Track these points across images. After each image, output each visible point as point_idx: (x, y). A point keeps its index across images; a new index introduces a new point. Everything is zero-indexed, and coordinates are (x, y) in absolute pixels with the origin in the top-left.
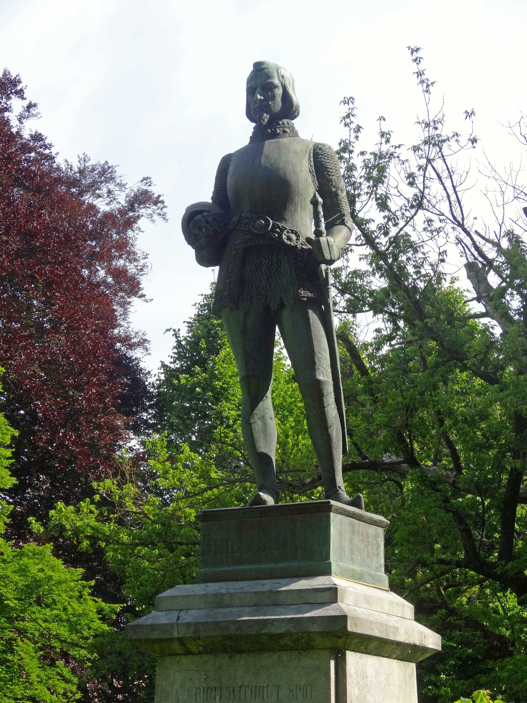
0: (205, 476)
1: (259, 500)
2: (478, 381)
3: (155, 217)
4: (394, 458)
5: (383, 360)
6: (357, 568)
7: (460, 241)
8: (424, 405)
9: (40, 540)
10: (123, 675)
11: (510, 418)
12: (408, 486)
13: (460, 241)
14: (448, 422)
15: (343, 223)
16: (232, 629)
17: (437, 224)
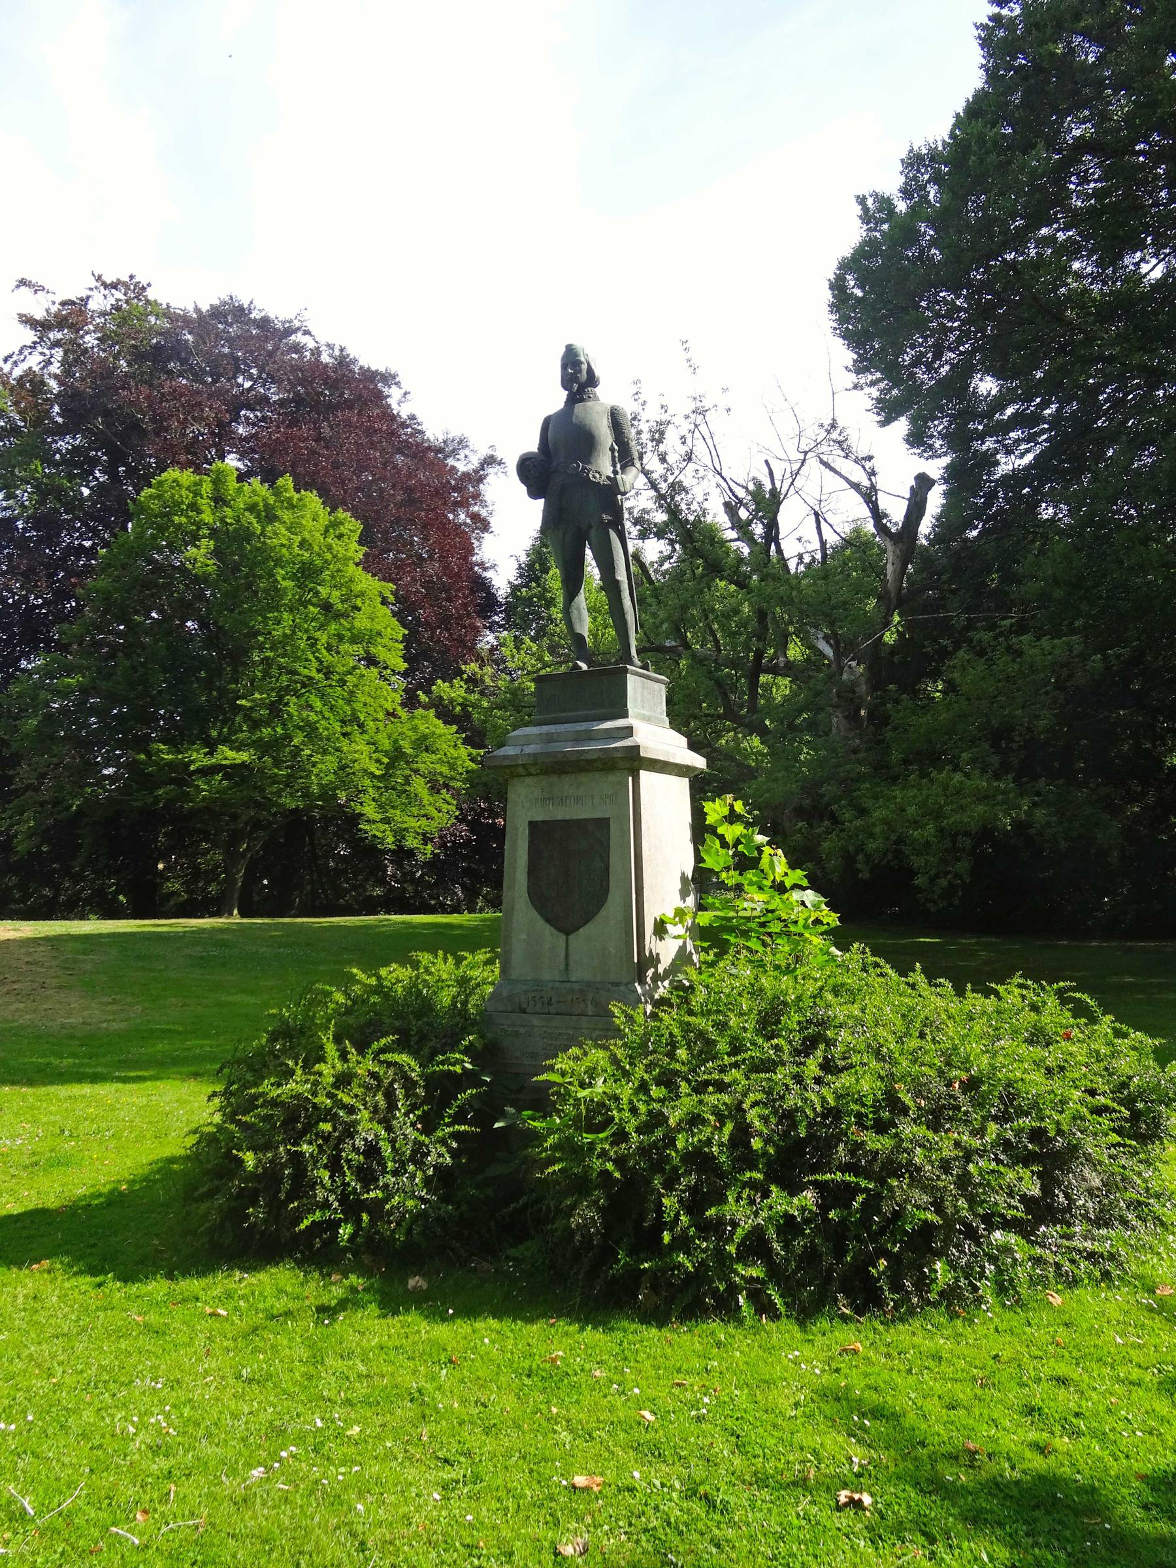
0: (540, 659)
1: (577, 667)
2: (733, 587)
3: (500, 474)
4: (673, 643)
5: (664, 574)
6: (647, 713)
7: (718, 486)
8: (695, 605)
9: (426, 707)
10: (487, 799)
11: (754, 613)
12: (683, 663)
13: (718, 486)
14: (711, 617)
15: (633, 465)
16: (560, 756)
17: (701, 473)
